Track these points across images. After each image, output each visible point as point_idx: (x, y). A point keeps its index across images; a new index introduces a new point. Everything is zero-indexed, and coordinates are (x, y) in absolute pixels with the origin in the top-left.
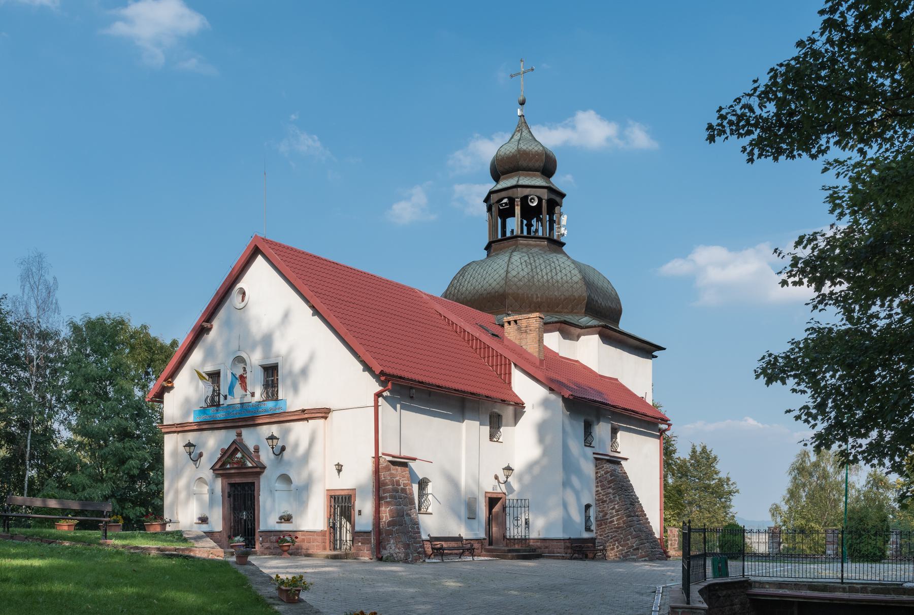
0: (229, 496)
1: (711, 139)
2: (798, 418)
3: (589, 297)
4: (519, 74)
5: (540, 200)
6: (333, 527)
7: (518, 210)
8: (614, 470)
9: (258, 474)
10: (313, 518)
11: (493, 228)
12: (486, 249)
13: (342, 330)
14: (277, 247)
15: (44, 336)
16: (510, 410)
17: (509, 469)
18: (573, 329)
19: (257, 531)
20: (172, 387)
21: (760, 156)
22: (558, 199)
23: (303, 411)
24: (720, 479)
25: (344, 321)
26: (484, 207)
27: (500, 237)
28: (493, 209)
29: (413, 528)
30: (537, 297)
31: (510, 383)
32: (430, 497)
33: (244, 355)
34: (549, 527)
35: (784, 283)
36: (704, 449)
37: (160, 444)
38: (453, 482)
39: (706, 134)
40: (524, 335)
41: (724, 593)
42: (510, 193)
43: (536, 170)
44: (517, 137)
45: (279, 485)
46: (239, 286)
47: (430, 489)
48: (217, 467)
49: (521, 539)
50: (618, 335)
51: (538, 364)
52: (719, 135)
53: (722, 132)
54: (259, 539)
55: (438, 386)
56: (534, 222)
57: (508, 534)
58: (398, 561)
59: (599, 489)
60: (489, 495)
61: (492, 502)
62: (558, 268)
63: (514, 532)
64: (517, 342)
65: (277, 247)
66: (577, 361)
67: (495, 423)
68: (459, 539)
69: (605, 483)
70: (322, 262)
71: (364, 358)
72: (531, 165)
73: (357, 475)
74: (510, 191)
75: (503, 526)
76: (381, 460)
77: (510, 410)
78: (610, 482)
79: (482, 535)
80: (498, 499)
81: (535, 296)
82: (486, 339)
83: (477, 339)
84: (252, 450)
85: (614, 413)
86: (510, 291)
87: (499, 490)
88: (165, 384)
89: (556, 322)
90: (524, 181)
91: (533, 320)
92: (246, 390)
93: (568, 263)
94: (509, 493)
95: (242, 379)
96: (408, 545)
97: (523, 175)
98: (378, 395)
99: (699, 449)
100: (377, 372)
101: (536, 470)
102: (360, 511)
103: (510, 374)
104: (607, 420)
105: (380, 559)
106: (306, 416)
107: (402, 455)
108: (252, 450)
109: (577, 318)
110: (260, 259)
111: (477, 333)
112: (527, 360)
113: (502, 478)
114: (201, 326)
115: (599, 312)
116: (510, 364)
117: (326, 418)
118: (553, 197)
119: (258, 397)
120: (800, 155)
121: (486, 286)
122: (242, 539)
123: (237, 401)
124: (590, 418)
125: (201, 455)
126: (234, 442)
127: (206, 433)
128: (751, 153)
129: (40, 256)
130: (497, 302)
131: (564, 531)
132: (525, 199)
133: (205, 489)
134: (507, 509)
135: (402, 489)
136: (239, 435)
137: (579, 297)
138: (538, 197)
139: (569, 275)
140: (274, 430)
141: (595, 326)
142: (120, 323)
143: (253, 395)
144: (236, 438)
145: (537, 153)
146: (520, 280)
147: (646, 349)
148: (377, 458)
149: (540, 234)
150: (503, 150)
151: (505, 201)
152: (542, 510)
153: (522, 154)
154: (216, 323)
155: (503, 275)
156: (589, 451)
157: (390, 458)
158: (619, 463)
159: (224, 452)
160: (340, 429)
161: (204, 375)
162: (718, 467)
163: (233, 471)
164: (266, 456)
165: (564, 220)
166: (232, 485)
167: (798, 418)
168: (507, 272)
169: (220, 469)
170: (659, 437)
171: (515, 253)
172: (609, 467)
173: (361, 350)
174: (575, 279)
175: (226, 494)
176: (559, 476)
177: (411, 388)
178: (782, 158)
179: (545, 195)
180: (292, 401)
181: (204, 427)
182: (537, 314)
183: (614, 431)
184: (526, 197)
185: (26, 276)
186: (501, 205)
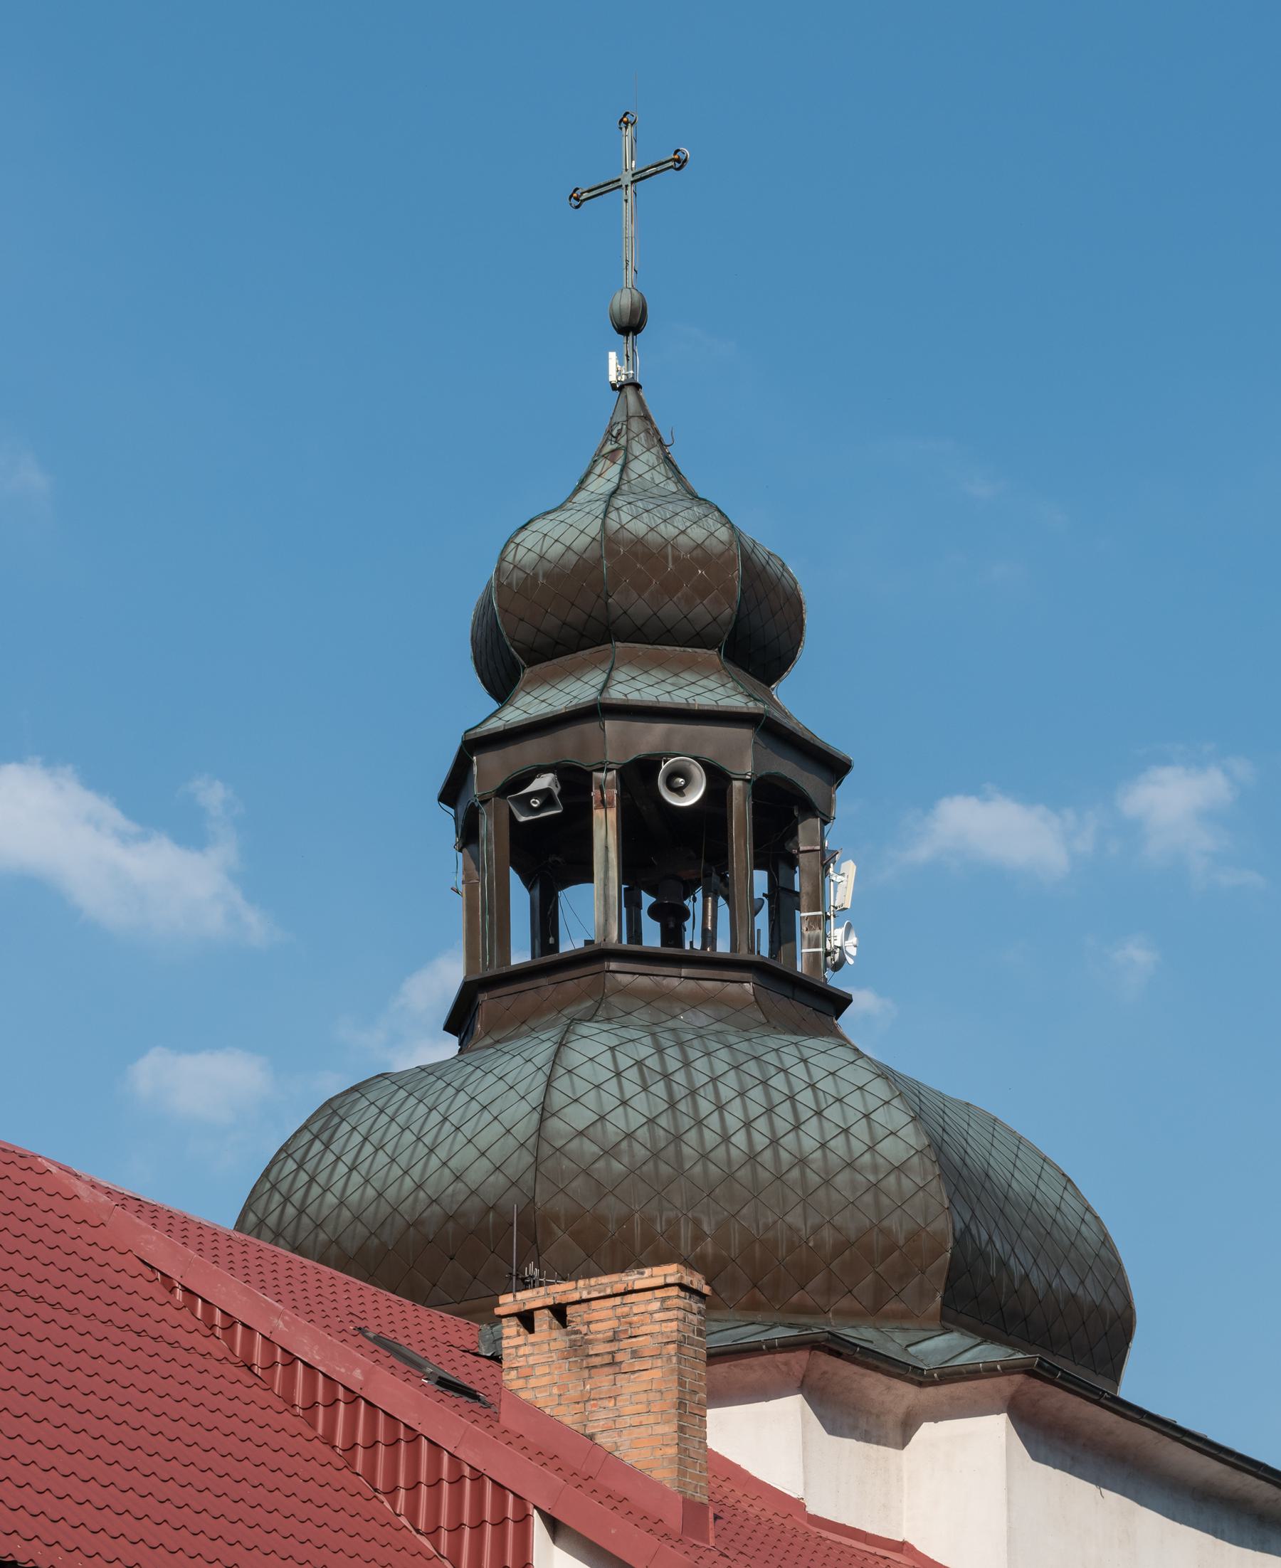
3: (962, 1238)
4: (613, 185)
5: (718, 778)
7: (605, 828)
11: (487, 923)
26: (445, 822)
27: (520, 955)
28: (486, 825)
30: (699, 1237)
40: (603, 1380)
42: (566, 744)
43: (699, 639)
44: (600, 485)
51: (674, 1520)
56: (695, 904)
62: (806, 1097)
64: (568, 1417)
72: (670, 610)
82: (401, 1396)
83: (353, 1398)
86: (560, 1205)
89: (788, 1346)
90: (634, 687)
91: (648, 1306)
93: (859, 1075)
97: (631, 661)
109: (900, 1338)
111: (354, 1369)
112: (618, 1501)
116: (523, 1521)
130: (465, 1258)
137: (913, 1236)
139: (860, 1129)
145: (701, 556)
146: (610, 1152)
149: (723, 947)
150: (529, 539)
151: (544, 782)
153: (621, 558)
155: (525, 1129)
165: (843, 885)
168: (544, 1112)
171: (584, 1029)
174: (892, 1150)
179: (744, 757)
182: (671, 1272)
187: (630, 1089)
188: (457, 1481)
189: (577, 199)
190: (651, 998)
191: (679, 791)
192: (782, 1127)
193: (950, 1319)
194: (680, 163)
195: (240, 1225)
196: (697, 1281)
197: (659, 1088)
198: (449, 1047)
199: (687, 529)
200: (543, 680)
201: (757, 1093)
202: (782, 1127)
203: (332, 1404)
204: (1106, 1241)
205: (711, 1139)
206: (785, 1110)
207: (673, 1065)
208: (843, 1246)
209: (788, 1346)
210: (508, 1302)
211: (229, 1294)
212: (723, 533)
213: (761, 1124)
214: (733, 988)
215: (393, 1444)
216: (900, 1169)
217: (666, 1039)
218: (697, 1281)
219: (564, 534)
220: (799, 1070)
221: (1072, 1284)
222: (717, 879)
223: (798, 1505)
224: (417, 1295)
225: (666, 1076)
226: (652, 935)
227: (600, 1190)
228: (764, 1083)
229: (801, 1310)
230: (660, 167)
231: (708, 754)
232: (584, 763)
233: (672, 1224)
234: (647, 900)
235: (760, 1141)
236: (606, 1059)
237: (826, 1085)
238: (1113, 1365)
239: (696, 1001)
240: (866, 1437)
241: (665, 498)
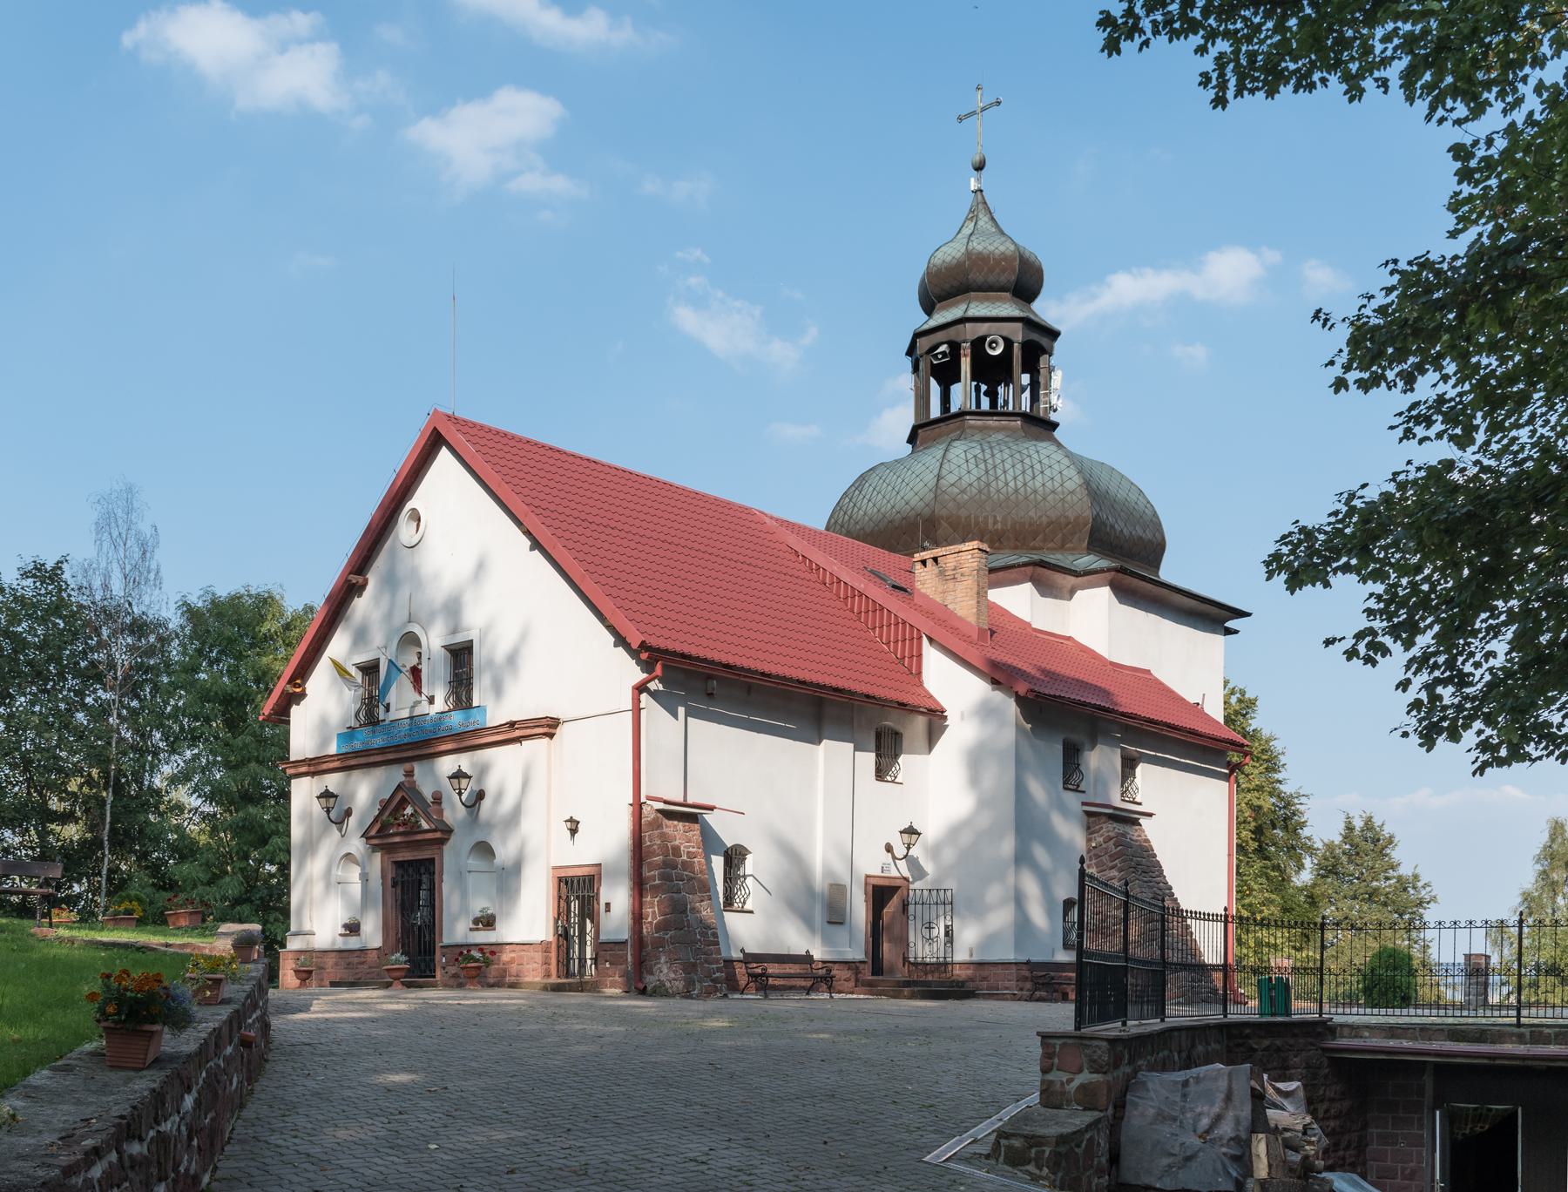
0: (394, 885)
1: (1112, 47)
2: (1351, 654)
4: (974, 113)
5: (1009, 343)
6: (564, 936)
7: (966, 365)
8: (1124, 835)
9: (441, 842)
10: (529, 921)
12: (909, 441)
13: (576, 572)
14: (474, 432)
15: (139, 627)
16: (920, 722)
17: (911, 831)
18: (1059, 578)
19: (438, 945)
20: (303, 695)
21: (1239, 93)
22: (1044, 341)
23: (512, 724)
24: (1399, 879)
25: (581, 556)
26: (908, 362)
27: (935, 411)
29: (704, 934)
30: (995, 522)
31: (919, 673)
32: (749, 881)
33: (417, 629)
34: (989, 940)
35: (1340, 384)
36: (1369, 824)
37: (285, 795)
38: (794, 857)
39: (1100, 36)
40: (951, 584)
41: (1266, 1042)
43: (1002, 289)
45: (473, 863)
46: (409, 505)
47: (749, 866)
48: (373, 833)
49: (938, 964)
50: (1149, 586)
51: (975, 636)
52: (1130, 37)
53: (1133, 30)
54: (441, 960)
55: (763, 674)
56: (1001, 390)
57: (911, 955)
58: (673, 996)
61: (881, 894)
62: (1037, 466)
63: (923, 950)
64: (938, 599)
65: (474, 432)
66: (1069, 638)
67: (887, 749)
68: (807, 959)
70: (564, 457)
71: (613, 622)
72: (991, 279)
73: (606, 841)
74: (952, 330)
75: (903, 942)
76: (646, 810)
77: (920, 722)
78: (1113, 857)
79: (857, 953)
80: (893, 890)
81: (990, 521)
82: (878, 593)
83: (861, 595)
84: (430, 799)
85: (1126, 729)
86: (944, 513)
88: (290, 689)
89: (1025, 565)
90: (977, 310)
91: (967, 556)
92: (419, 690)
93: (1058, 456)
94: (915, 880)
95: (416, 673)
96: (694, 965)
97: (977, 299)
98: (640, 688)
99: (1358, 824)
100: (635, 646)
101: (966, 839)
103: (920, 656)
104: (1114, 742)
105: (643, 992)
106: (518, 733)
107: (690, 801)
108: (430, 799)
109: (1071, 558)
110: (444, 454)
112: (954, 630)
113: (900, 851)
114: (347, 581)
115: (1127, 554)
117: (551, 736)
118: (1035, 337)
119: (440, 705)
120: (1324, 81)
121: (900, 505)
122: (404, 958)
123: (405, 714)
124: (1076, 737)
125: (348, 813)
126: (399, 787)
127: (356, 774)
128: (1222, 86)
129: (130, 489)
130: (913, 534)
131: (1018, 946)
132: (984, 343)
133: (354, 873)
134: (911, 908)
135: (684, 862)
136: (409, 774)
137: (1077, 518)
138: (1004, 339)
139: (1058, 478)
140: (464, 762)
141: (1102, 571)
142: (265, 603)
143: (431, 700)
144: (403, 779)
146: (963, 492)
147: (1212, 616)
148: (638, 806)
150: (939, 255)
151: (943, 348)
152: (978, 910)
153: (974, 260)
154: (373, 578)
155: (932, 484)
156: (1073, 800)
157: (661, 806)
158: (1135, 822)
159: (385, 805)
160: (577, 760)
161: (353, 671)
162: (1396, 854)
163: (397, 839)
164: (454, 812)
165: (1057, 379)
166: (399, 865)
167: (1351, 654)
168: (939, 477)
170: (1226, 778)
172: (1110, 828)
173: (606, 606)
174: (1070, 485)
175: (389, 882)
176: (1008, 846)
177: (710, 677)
178: (1286, 91)
179: (1017, 333)
180: (495, 710)
181: (353, 762)
182: (975, 544)
183: (1129, 764)
184: (982, 339)
185: (105, 524)
186: (935, 357)
187: (972, 466)
189: (960, 119)
190: (981, 429)
192: (1028, 478)
194: (999, 103)
195: (827, 529)
196: (985, 547)
197: (982, 466)
199: (998, 247)
200: (943, 308)
201: (1019, 466)
202: (1028, 478)
204: (1155, 514)
205: (1001, 484)
206: (1029, 472)
208: (1050, 523)
210: (918, 556)
211: (818, 557)
212: (1012, 248)
216: (1072, 492)
217: (986, 446)
218: (985, 547)
219: (953, 252)
220: (1035, 456)
221: (1140, 532)
222: (1008, 378)
224: (892, 549)
226: (985, 404)
227: (959, 507)
229: (1034, 548)
230: (991, 105)
232: (958, 339)
233: (986, 518)
234: (984, 388)
235: (1020, 484)
237: (1046, 461)
238: (1155, 562)
239: (998, 430)
240: (1056, 597)
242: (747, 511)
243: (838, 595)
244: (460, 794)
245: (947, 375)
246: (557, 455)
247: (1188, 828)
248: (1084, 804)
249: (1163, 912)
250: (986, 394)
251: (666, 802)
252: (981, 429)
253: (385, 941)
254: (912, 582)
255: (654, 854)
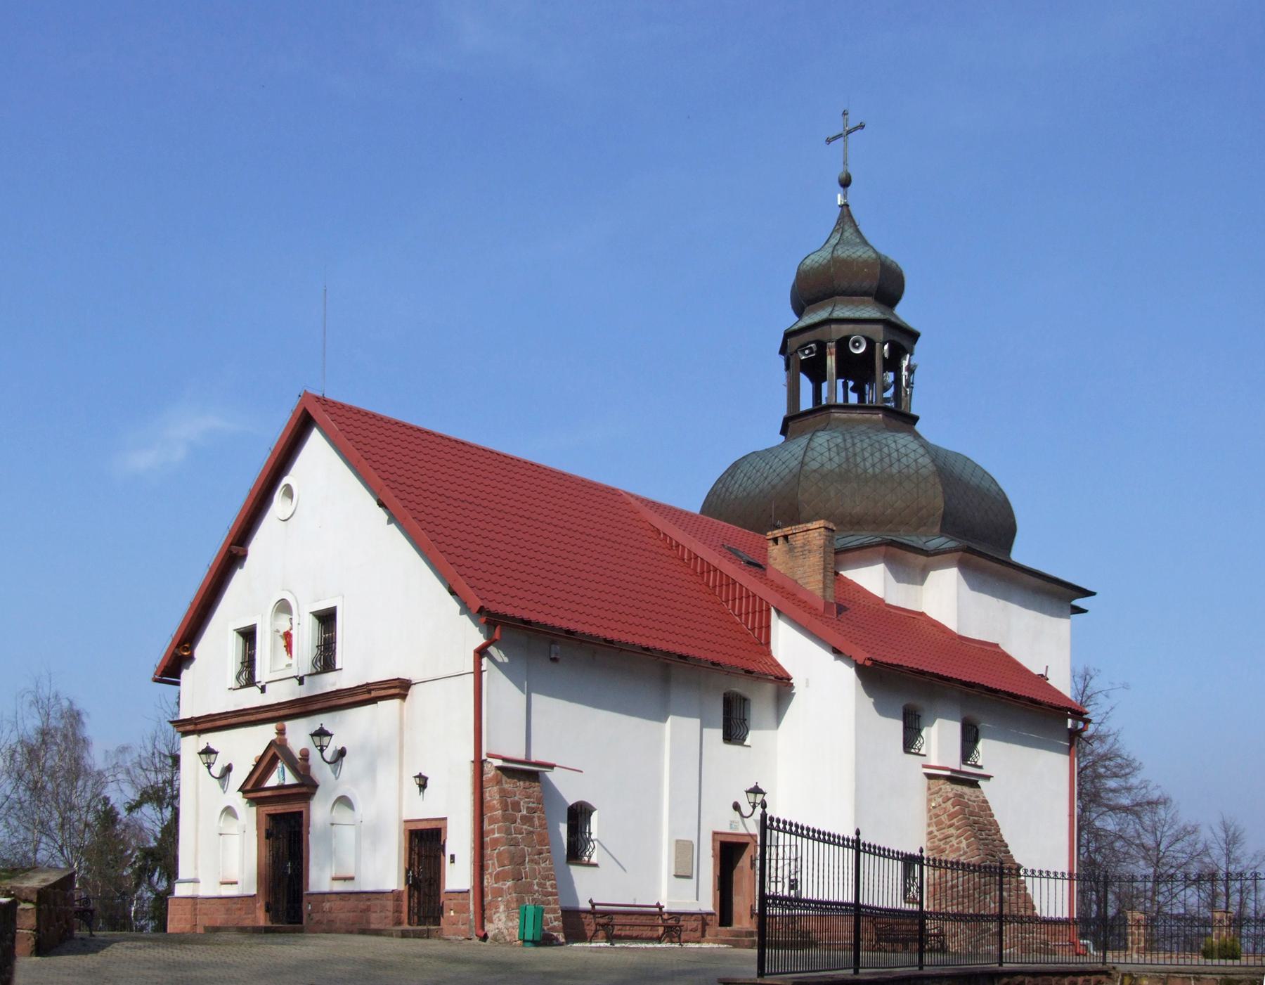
5: (871, 343)
7: (831, 362)
17: (756, 790)
19: (442, 892)
22: (905, 343)
27: (806, 403)
31: (768, 643)
46: (286, 480)
47: (595, 826)
48: (248, 787)
59: (934, 828)
60: (723, 838)
62: (895, 455)
66: (922, 614)
69: (944, 818)
76: (487, 767)
83: (715, 570)
84: (298, 756)
87: (742, 830)
89: (879, 544)
93: (914, 445)
98: (481, 653)
102: (452, 857)
103: (768, 627)
106: (374, 694)
107: (533, 759)
108: (298, 756)
111: (714, 559)
115: (978, 534)
116: (768, 611)
117: (403, 697)
126: (272, 744)
136: (281, 732)
144: (274, 736)
145: (866, 263)
147: (1061, 595)
148: (479, 764)
150: (808, 262)
157: (499, 763)
158: (974, 784)
168: (802, 463)
169: (253, 789)
175: (264, 834)
179: (878, 332)
182: (821, 523)
184: (847, 339)
187: (833, 454)
188: (748, 597)
191: (857, 348)
193: (944, 531)
195: (702, 511)
196: (831, 526)
198: (782, 438)
199: (860, 253)
203: (709, 572)
207: (849, 445)
209: (879, 544)
210: (770, 535)
213: (878, 465)
214: (875, 417)
215: (728, 585)
217: (848, 436)
220: (893, 445)
223: (882, 600)
225: (846, 449)
228: (880, 450)
231: (867, 334)
232: (825, 339)
234: (851, 384)
236: (826, 445)
237: (903, 450)
241: (856, 245)
242: (614, 492)
243: (695, 569)
244: (322, 751)
245: (816, 371)
246: (424, 436)
247: (1030, 797)
248: (925, 766)
249: (999, 869)
250: (853, 390)
251: (504, 759)
252: (845, 421)
253: (258, 890)
254: (765, 556)
255: (493, 809)
